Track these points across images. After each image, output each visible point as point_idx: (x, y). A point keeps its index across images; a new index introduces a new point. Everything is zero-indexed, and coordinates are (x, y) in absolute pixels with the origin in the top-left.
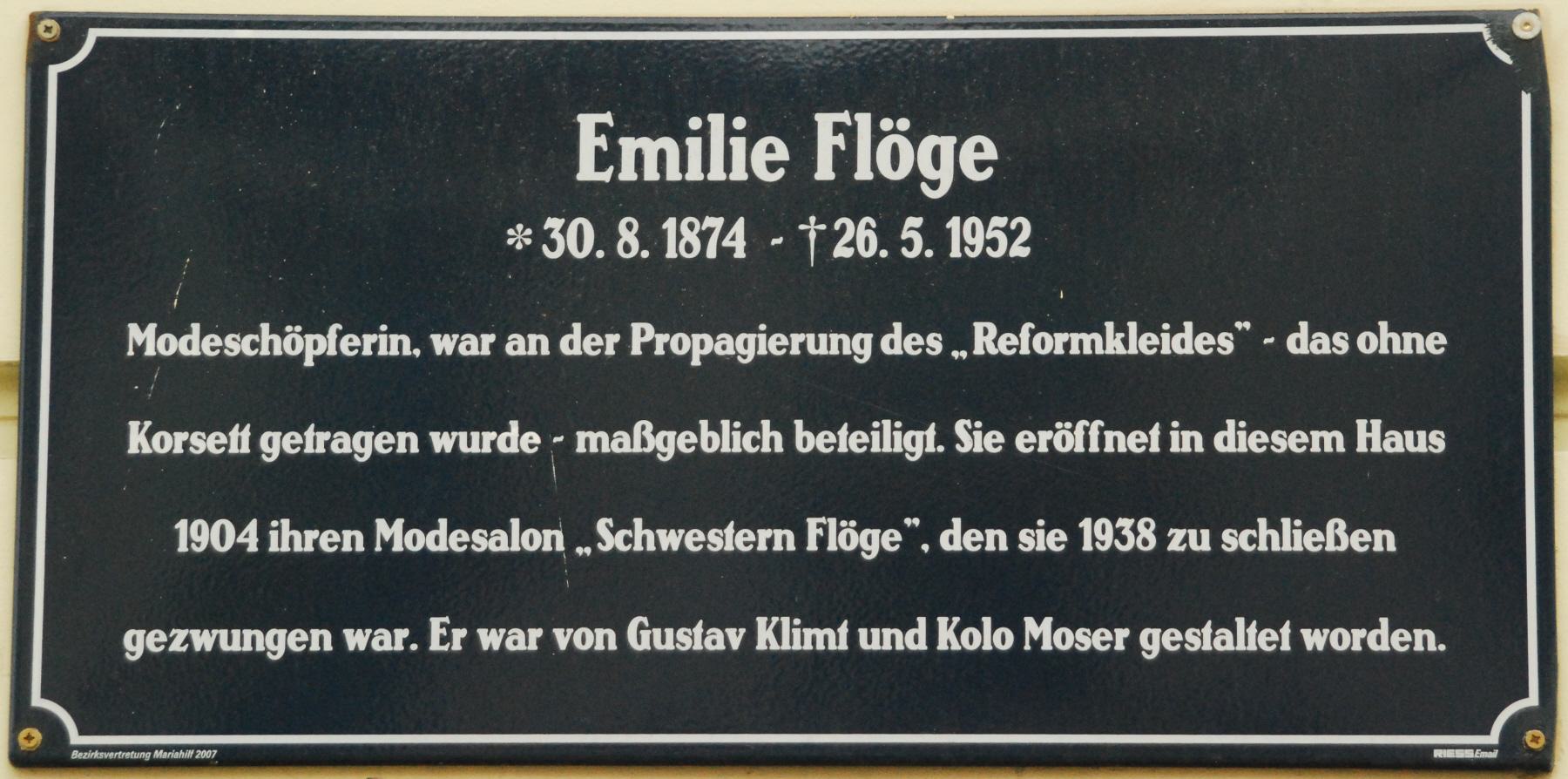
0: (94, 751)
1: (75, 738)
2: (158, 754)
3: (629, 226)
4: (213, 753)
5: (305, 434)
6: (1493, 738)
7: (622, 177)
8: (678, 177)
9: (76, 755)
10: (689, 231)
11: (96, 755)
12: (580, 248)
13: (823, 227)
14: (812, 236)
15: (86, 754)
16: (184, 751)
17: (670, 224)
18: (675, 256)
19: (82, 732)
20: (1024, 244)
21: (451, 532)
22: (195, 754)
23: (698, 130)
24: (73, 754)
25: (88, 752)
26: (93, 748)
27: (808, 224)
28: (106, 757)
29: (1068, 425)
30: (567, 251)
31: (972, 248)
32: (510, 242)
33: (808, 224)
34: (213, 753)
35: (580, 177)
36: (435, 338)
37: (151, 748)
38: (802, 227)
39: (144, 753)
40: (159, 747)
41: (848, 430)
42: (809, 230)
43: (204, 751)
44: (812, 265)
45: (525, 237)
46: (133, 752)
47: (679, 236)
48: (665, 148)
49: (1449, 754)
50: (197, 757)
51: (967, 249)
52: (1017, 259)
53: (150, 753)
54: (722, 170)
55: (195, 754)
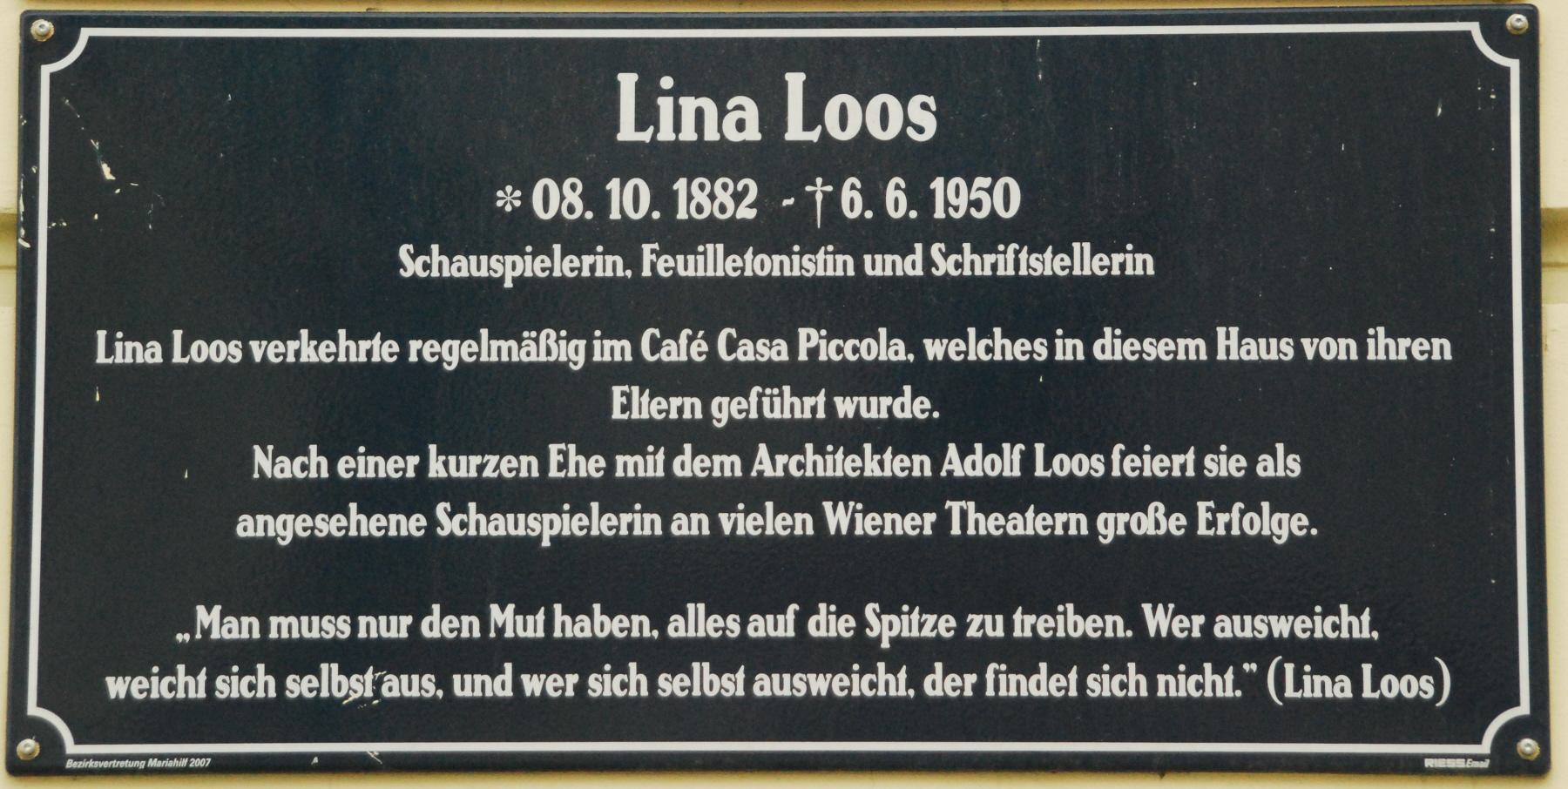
0: (88, 760)
1: (71, 747)
2: (153, 763)
3: (573, 187)
4: (207, 762)
5: (1361, 617)
6: (1485, 747)
7: (661, 137)
8: (671, 137)
9: (70, 764)
10: (723, 192)
11: (91, 764)
12: (1007, 208)
13: (829, 188)
14: (819, 197)
15: (81, 763)
16: (179, 760)
17: (681, 185)
18: (686, 217)
19: (78, 741)
20: (750, 206)
21: (1051, 676)
22: (189, 763)
23: (670, 90)
24: (68, 763)
25: (82, 760)
26: (88, 757)
27: (815, 185)
28: (100, 766)
29: (534, 334)
30: (993, 211)
31: (956, 209)
32: (500, 203)
33: (815, 185)
34: (207, 762)
35: (621, 137)
36: (927, 342)
37: (145, 757)
38: (809, 188)
39: (138, 762)
40: (153, 756)
41: (381, 339)
42: (815, 192)
43: (198, 759)
44: (819, 227)
45: (511, 194)
46: (127, 761)
47: (690, 198)
48: (703, 106)
49: (1440, 763)
50: (191, 765)
51: (951, 210)
52: (744, 221)
53: (144, 762)
54: (757, 129)
55: (189, 763)
